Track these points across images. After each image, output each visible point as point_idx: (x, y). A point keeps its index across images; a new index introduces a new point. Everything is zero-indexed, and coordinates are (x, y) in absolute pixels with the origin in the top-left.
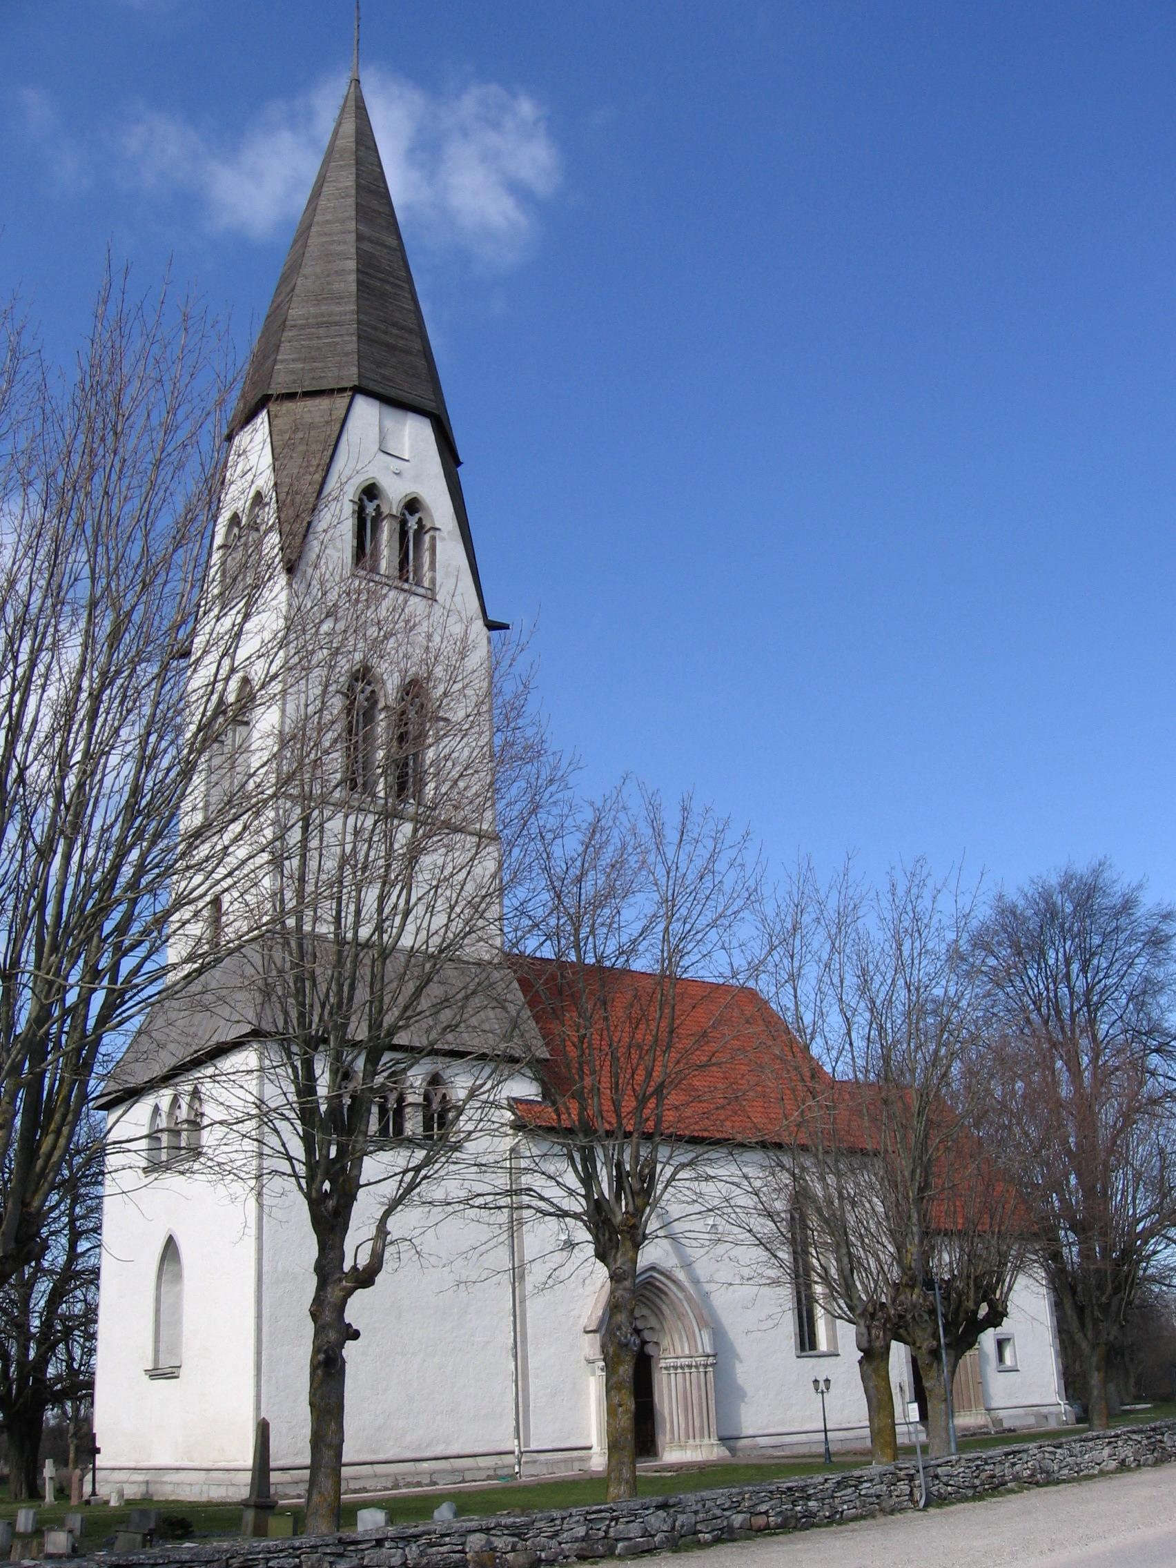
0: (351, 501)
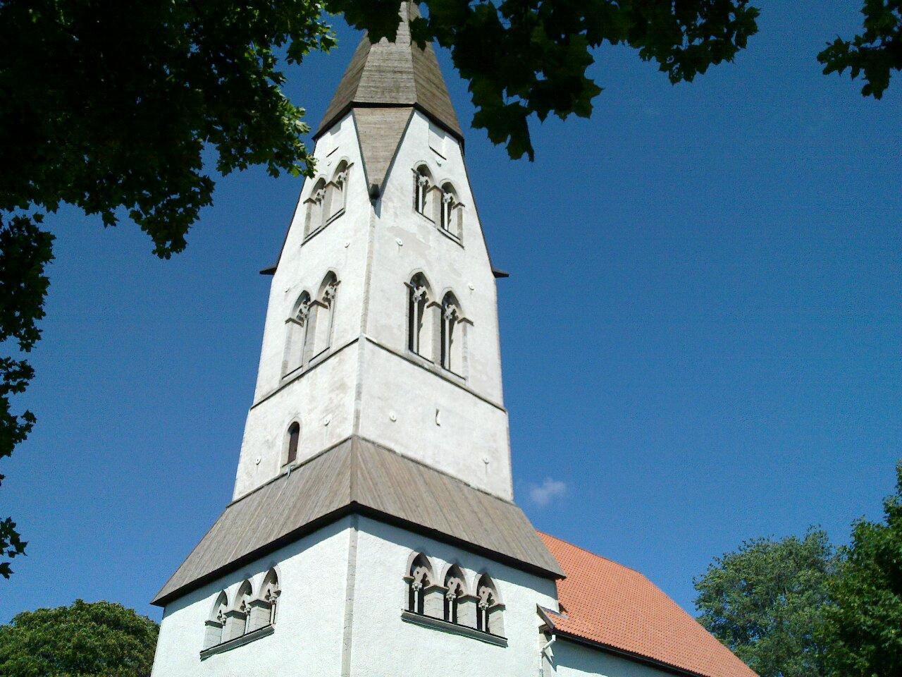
0: (208, 623)
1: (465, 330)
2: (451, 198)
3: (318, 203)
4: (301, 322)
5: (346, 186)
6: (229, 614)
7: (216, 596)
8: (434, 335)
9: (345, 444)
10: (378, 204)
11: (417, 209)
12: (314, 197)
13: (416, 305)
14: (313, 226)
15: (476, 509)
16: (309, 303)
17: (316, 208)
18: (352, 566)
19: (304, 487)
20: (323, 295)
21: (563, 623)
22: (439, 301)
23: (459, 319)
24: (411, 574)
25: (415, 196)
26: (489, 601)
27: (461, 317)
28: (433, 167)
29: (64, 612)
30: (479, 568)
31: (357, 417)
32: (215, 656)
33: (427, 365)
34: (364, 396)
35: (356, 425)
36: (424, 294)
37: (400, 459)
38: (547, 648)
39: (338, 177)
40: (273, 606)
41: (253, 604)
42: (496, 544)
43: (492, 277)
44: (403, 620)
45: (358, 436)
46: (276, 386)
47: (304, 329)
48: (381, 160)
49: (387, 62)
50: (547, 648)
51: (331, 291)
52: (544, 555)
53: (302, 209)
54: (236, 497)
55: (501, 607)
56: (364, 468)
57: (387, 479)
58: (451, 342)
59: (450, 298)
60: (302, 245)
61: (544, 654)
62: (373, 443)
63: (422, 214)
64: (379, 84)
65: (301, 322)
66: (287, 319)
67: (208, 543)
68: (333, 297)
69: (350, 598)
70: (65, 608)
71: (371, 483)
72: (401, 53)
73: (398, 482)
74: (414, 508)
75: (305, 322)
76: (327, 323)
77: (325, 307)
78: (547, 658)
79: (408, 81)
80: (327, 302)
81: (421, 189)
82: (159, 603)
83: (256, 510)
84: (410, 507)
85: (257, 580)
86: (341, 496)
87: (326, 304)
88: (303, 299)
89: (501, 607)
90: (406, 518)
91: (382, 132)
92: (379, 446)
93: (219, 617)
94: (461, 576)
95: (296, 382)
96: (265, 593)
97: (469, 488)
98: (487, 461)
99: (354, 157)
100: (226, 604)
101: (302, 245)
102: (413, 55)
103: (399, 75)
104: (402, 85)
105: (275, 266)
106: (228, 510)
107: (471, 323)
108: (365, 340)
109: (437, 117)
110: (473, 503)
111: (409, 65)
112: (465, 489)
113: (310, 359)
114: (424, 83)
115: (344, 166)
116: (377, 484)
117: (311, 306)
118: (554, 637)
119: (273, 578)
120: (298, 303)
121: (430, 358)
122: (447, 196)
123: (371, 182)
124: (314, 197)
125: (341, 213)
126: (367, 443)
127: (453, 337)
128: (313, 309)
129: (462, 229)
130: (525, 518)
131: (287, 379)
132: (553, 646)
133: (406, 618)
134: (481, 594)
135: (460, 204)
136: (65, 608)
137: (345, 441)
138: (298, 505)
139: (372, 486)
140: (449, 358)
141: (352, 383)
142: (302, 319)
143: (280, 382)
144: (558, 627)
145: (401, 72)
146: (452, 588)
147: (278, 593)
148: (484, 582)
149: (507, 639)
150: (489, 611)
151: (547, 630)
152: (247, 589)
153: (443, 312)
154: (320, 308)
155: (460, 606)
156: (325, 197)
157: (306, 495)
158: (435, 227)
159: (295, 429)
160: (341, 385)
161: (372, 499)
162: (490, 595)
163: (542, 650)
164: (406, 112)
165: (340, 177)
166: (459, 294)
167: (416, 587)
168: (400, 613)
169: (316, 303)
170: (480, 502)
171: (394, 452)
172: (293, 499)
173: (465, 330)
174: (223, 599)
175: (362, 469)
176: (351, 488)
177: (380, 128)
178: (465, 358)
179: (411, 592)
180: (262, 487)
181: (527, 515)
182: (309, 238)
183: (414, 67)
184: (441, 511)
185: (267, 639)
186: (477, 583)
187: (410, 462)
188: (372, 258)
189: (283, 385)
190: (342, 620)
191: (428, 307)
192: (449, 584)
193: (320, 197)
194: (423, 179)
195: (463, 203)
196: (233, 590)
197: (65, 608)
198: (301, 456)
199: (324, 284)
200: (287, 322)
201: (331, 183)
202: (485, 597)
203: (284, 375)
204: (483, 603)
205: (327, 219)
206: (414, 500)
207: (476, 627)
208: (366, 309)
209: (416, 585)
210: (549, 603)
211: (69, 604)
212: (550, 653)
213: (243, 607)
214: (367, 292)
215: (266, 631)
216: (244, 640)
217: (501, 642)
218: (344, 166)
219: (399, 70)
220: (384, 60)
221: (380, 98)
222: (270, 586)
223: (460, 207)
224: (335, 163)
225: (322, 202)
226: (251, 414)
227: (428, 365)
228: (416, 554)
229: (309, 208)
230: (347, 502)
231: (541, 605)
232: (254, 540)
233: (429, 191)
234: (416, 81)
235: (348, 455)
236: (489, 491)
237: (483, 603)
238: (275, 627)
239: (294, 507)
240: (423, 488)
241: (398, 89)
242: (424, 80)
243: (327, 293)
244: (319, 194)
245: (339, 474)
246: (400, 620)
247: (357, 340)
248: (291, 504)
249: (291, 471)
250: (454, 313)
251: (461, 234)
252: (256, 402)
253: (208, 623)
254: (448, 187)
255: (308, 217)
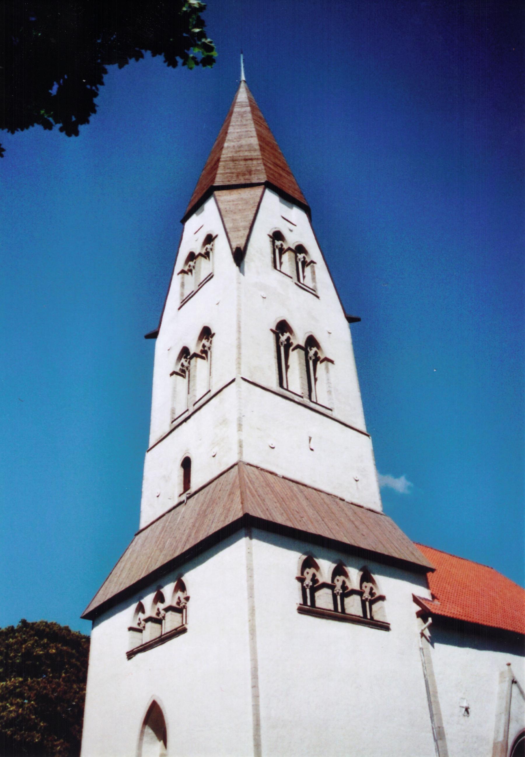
0: (131, 629)
1: (327, 368)
2: (304, 258)
3: (190, 273)
4: (184, 374)
5: (213, 257)
6: (147, 620)
7: (134, 606)
8: (301, 373)
9: (232, 470)
10: (242, 265)
11: (275, 267)
12: (186, 268)
13: (282, 349)
14: (187, 293)
15: (352, 518)
16: (188, 357)
17: (188, 278)
18: (250, 569)
19: (200, 510)
20: (201, 348)
21: (436, 607)
22: (302, 344)
23: (321, 359)
24: (302, 573)
25: (272, 256)
26: (372, 594)
27: (322, 357)
28: (285, 233)
29: (11, 630)
30: (360, 567)
31: (241, 446)
32: (140, 656)
33: (297, 399)
34: (245, 428)
35: (241, 453)
36: (288, 339)
37: (282, 480)
38: (425, 629)
39: (205, 248)
40: (184, 610)
41: (167, 610)
42: (373, 544)
43: (344, 323)
44: (299, 613)
45: (242, 462)
46: (168, 430)
47: (186, 380)
48: (241, 229)
49: (238, 153)
50: (425, 629)
51: (207, 344)
52: (414, 552)
53: (176, 280)
54: (142, 525)
55: (382, 598)
56: (251, 487)
57: (272, 496)
58: (316, 380)
59: (312, 341)
60: (179, 309)
61: (422, 635)
62: (257, 467)
63: (280, 271)
64: (233, 171)
65: (184, 374)
66: (171, 372)
67: (123, 564)
68: (209, 348)
69: (251, 596)
70: (13, 627)
71: (259, 499)
72: (250, 145)
73: (282, 498)
74: (299, 518)
75: (187, 373)
76: (206, 372)
77: (203, 358)
78: (426, 637)
79: (258, 166)
80: (204, 354)
81: (277, 251)
82: (87, 617)
83: (160, 533)
84: (296, 518)
85: (168, 590)
86: (233, 512)
87: (204, 355)
88: (183, 355)
89: (382, 598)
90: (292, 526)
91: (240, 207)
92: (262, 469)
93: (139, 624)
94: (346, 575)
95: (184, 424)
96: (176, 600)
97: (344, 502)
98: (357, 479)
99: (217, 229)
100: (143, 612)
101: (179, 309)
102: (260, 146)
103: (249, 162)
104: (253, 169)
105: (157, 330)
106: (137, 537)
107: (332, 362)
108: (241, 380)
109: (286, 191)
110: (349, 513)
111: (257, 154)
112: (341, 503)
113: (193, 403)
114: (272, 167)
115: (209, 239)
116: (264, 500)
117: (191, 358)
118: (430, 620)
119: (181, 587)
120: (179, 358)
121: (299, 394)
122: (301, 256)
123: (234, 246)
124: (186, 268)
125: (210, 277)
126: (252, 468)
127: (317, 375)
128: (193, 361)
129: (316, 283)
130: (395, 525)
131: (176, 423)
132: (430, 627)
133: (302, 610)
134: (364, 588)
135: (312, 262)
136: (13, 627)
137: (232, 467)
138: (197, 525)
139: (260, 502)
140: (316, 396)
141: (233, 418)
142: (183, 371)
143: (170, 426)
144: (433, 611)
145: (251, 159)
146: (339, 584)
147: (187, 599)
148: (366, 578)
149: (389, 624)
150: (372, 602)
151: (423, 614)
152: (160, 598)
153: (307, 354)
154: (199, 360)
155: (347, 600)
156: (196, 268)
157: (203, 515)
158: (292, 281)
159: (186, 464)
160: (224, 421)
161: (262, 512)
162: (372, 589)
163: (420, 631)
164: (258, 191)
165: (207, 249)
166: (320, 338)
167: (307, 585)
168: (296, 607)
169: (195, 355)
170: (355, 513)
171: (276, 475)
172: (192, 520)
173: (327, 368)
174: (141, 609)
175: (249, 488)
176: (242, 503)
177: (237, 204)
178: (329, 392)
179: (304, 590)
180: (163, 515)
181: (396, 522)
182: (184, 302)
183: (262, 155)
184: (323, 520)
185: (182, 637)
186: (359, 578)
187: (291, 482)
188: (240, 309)
189: (173, 427)
190: (246, 616)
191: (293, 350)
192: (335, 581)
193: (191, 268)
194: (278, 243)
195: (315, 260)
196: (148, 600)
197: (13, 627)
198: (194, 485)
199: (200, 338)
200: (172, 374)
201: (200, 254)
202: (367, 591)
203: (173, 420)
204: (366, 595)
205: (199, 284)
206: (298, 512)
207: (361, 615)
208: (240, 353)
209: (307, 583)
210: (423, 593)
211: (16, 624)
212: (427, 633)
213: (158, 614)
214: (239, 338)
215: (181, 631)
216: (162, 640)
217: (385, 627)
218: (209, 239)
219: (250, 157)
220: (236, 152)
221: (235, 181)
222: (180, 594)
223: (312, 264)
224: (202, 237)
225: (194, 271)
226: (149, 456)
227: (298, 399)
228: (304, 557)
229: (183, 278)
230: (240, 515)
231: (417, 594)
232: (162, 557)
233: (285, 252)
234: (265, 165)
235: (236, 478)
236: (361, 504)
237: (366, 595)
238: (187, 626)
239: (194, 526)
240: (304, 503)
241: (250, 172)
242: (270, 164)
243: (204, 346)
244: (190, 266)
245: (230, 495)
246: (296, 612)
247: (233, 381)
248: (190, 525)
249: (188, 498)
250: (316, 354)
251: (315, 286)
252: (151, 445)
253: (131, 629)
254: (300, 249)
255: (183, 285)
